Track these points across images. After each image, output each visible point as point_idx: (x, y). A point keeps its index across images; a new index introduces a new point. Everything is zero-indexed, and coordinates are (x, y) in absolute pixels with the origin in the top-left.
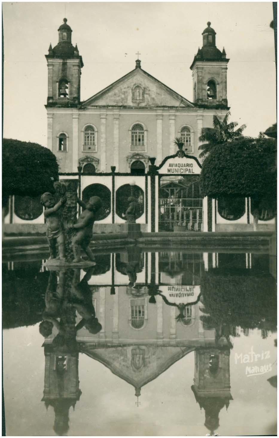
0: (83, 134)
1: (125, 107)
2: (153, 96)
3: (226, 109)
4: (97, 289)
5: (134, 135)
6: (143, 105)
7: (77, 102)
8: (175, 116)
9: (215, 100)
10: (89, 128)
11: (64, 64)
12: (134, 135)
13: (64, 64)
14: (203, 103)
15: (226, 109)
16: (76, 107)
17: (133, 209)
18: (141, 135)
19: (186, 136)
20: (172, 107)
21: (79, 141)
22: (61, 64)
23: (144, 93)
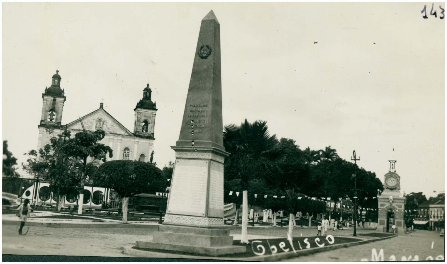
8: (121, 140)
11: (54, 100)
12: (125, 153)
13: (54, 100)
14: (139, 134)
16: (59, 129)
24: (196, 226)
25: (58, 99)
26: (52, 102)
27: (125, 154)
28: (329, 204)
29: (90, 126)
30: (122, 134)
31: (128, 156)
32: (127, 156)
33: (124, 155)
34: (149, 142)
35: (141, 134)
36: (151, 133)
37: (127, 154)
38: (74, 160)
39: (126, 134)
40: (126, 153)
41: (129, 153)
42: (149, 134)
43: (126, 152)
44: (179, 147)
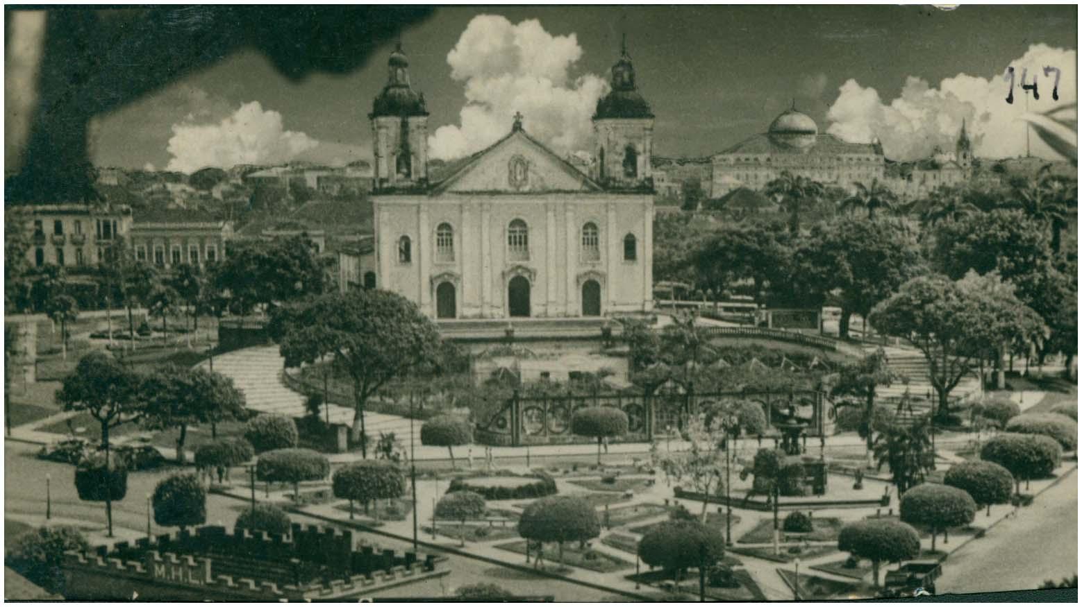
0: (435, 236)
1: (495, 193)
2: (543, 174)
3: (242, 103)
4: (280, 422)
5: (513, 235)
6: (526, 189)
7: (425, 186)
8: (575, 205)
9: (634, 181)
10: (445, 226)
11: (404, 125)
12: (513, 235)
13: (404, 125)
14: (617, 185)
15: (242, 103)
16: (425, 194)
17: (963, 529)
18: (523, 235)
19: (590, 236)
20: (572, 192)
21: (419, 250)
22: (399, 125)
23: (526, 170)
24: (579, 343)
25: (414, 121)
26: (399, 131)
27: (515, 237)
28: (260, 305)
29: (495, 180)
30: (575, 189)
31: (523, 240)
32: (520, 243)
33: (523, 240)
34: (641, 201)
35: (621, 185)
36: (647, 179)
37: (520, 237)
38: (899, 252)
39: (587, 189)
40: (444, 237)
41: (450, 235)
42: (639, 181)
43: (515, 232)
44: (140, 229)
